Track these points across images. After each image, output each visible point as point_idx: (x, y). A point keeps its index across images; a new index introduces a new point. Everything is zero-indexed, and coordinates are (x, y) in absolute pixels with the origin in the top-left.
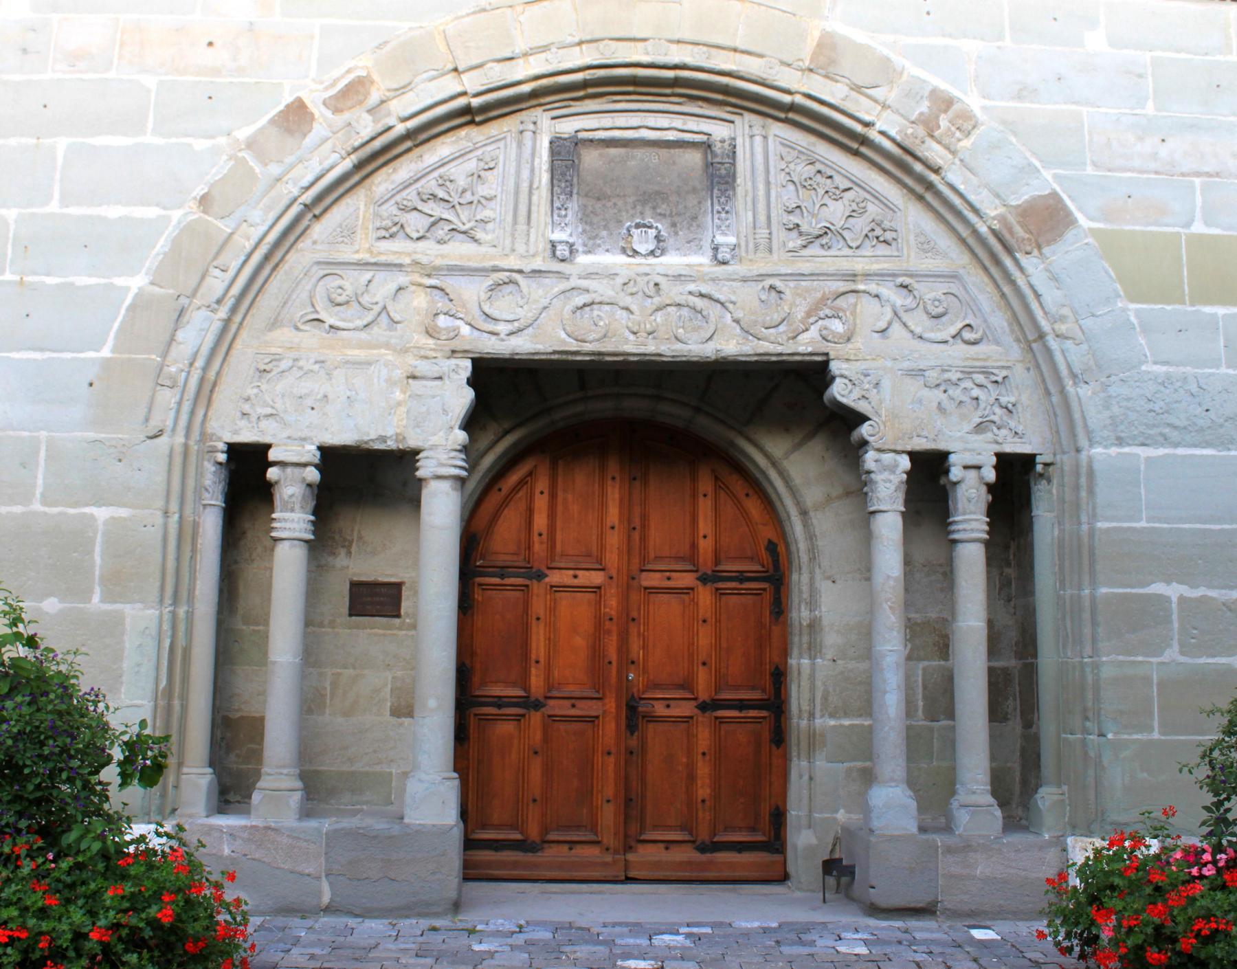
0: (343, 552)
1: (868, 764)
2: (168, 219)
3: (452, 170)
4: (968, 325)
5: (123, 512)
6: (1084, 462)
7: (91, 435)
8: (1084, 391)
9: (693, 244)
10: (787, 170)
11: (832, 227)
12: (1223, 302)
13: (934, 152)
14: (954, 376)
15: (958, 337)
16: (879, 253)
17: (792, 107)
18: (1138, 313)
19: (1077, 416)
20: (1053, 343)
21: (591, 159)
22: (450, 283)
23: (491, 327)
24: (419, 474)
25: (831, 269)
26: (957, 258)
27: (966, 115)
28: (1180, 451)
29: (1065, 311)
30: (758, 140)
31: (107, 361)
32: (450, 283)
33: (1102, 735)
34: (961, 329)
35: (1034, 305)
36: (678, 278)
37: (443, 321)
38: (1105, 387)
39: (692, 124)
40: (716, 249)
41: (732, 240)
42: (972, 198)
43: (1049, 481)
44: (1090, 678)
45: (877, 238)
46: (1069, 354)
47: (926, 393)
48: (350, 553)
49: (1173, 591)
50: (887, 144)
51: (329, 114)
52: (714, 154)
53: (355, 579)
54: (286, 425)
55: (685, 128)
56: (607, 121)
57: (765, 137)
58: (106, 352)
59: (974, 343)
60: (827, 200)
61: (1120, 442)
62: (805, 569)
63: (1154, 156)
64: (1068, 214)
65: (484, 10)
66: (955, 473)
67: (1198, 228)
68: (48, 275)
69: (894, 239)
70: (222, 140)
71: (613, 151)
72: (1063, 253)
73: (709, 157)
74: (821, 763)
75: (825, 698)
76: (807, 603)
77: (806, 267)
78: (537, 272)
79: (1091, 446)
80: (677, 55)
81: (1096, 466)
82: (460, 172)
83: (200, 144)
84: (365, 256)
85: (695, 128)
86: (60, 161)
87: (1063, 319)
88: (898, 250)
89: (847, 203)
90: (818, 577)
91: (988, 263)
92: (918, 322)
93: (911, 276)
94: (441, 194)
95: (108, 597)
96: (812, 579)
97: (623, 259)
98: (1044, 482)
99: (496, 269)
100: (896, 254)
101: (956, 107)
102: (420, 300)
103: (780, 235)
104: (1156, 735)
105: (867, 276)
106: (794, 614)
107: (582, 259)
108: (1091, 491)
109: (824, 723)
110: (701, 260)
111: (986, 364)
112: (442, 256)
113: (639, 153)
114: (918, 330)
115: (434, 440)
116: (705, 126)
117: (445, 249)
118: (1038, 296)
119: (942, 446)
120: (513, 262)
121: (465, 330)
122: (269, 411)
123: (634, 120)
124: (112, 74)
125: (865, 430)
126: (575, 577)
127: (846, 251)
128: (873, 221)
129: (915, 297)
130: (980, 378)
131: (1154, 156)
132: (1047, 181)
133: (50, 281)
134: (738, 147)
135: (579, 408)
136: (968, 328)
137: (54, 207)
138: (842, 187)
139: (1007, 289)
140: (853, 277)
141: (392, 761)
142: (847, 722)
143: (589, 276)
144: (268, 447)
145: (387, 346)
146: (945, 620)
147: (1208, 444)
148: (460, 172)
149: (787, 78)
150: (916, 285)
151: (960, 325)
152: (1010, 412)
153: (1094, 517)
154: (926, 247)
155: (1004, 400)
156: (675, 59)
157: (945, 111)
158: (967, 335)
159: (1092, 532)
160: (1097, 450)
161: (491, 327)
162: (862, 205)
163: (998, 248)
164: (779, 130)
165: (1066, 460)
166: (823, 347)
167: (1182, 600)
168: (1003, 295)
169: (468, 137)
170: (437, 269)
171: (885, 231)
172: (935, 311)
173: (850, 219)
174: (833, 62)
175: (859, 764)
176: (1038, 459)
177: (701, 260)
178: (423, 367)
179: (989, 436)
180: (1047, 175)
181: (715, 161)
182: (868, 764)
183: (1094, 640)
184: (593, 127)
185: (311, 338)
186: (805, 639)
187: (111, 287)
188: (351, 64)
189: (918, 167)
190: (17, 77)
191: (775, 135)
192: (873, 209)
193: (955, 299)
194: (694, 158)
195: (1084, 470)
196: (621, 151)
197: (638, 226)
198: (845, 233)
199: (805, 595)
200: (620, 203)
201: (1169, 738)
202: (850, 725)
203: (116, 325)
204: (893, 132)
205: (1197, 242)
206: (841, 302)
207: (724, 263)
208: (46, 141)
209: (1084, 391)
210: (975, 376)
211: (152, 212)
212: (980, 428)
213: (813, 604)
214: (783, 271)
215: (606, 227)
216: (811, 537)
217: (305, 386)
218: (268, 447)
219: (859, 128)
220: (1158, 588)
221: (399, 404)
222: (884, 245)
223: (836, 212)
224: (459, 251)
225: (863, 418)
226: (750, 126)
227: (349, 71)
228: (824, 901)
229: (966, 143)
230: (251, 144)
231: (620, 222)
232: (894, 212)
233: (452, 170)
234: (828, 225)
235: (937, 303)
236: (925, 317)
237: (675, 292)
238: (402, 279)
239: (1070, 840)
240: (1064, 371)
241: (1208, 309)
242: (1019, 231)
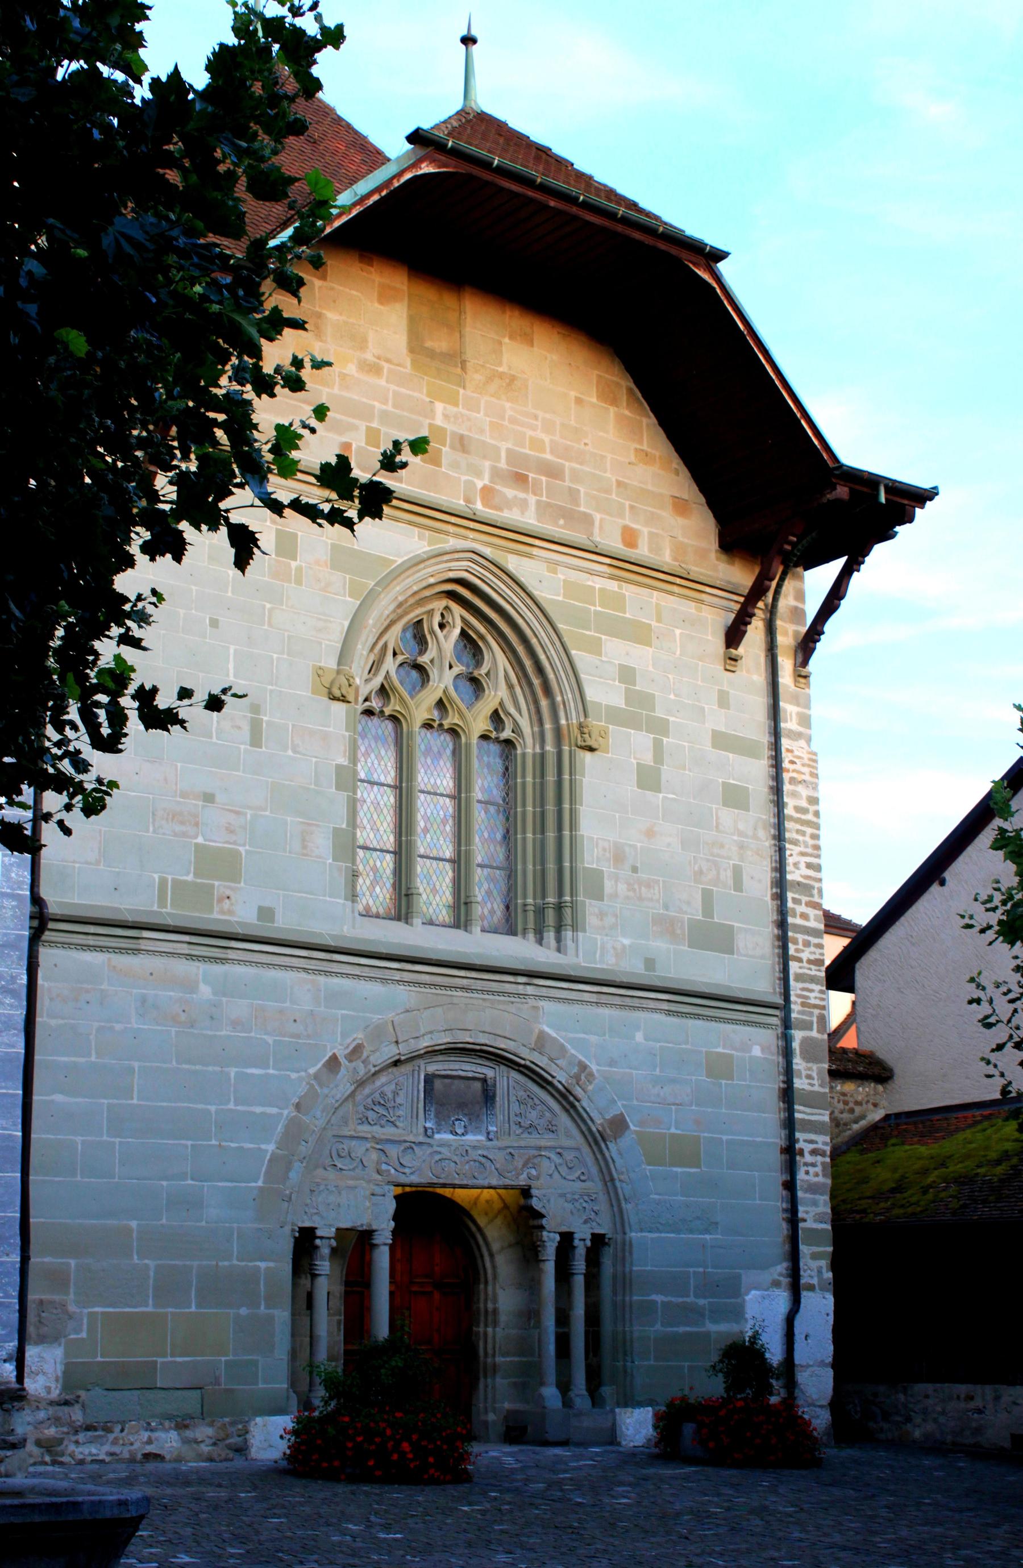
2: (282, 1114)
3: (385, 1089)
5: (271, 1264)
6: (627, 1239)
7: (256, 1225)
8: (629, 1206)
9: (477, 1130)
12: (680, 1166)
13: (578, 1091)
14: (576, 1197)
17: (525, 1066)
18: (650, 1170)
19: (626, 1217)
20: (618, 1184)
21: (438, 1084)
23: (402, 1170)
24: (374, 1242)
25: (533, 1145)
26: (580, 1140)
27: (591, 1075)
28: (663, 1235)
29: (624, 1170)
31: (260, 1188)
32: (388, 1148)
33: (633, 1362)
35: (612, 1166)
36: (474, 1147)
37: (384, 1167)
38: (637, 1205)
39: (480, 1069)
40: (488, 1133)
41: (495, 1129)
42: (592, 1115)
44: (628, 1337)
46: (624, 1189)
47: (566, 1204)
49: (659, 1298)
50: (560, 1087)
51: (347, 1062)
52: (487, 1085)
54: (322, 1217)
56: (446, 1066)
58: (260, 1183)
59: (584, 1181)
61: (642, 1231)
63: (658, 1095)
65: (408, 1011)
66: (576, 1242)
67: (673, 1130)
68: (232, 1142)
70: (303, 1074)
72: (626, 1141)
74: (498, 1380)
77: (522, 1143)
78: (421, 1143)
79: (631, 1231)
80: (483, 1039)
81: (633, 1242)
82: (388, 1090)
83: (294, 1076)
84: (352, 1133)
86: (233, 1081)
87: (622, 1173)
90: (497, 1287)
91: (592, 1144)
92: (563, 1170)
95: (267, 1307)
96: (494, 1289)
97: (451, 1137)
99: (405, 1141)
101: (588, 1070)
102: (374, 1156)
103: (514, 1127)
104: (652, 1362)
105: (546, 1148)
107: (437, 1136)
108: (631, 1253)
109: (499, 1359)
110: (482, 1138)
113: (456, 1082)
114: (564, 1174)
115: (384, 1226)
117: (384, 1130)
118: (614, 1161)
119: (572, 1230)
120: (411, 1138)
121: (393, 1171)
122: (315, 1211)
123: (457, 1066)
124: (252, 1034)
125: (544, 1222)
127: (538, 1136)
130: (586, 1198)
131: (658, 1095)
132: (619, 1107)
133: (233, 1145)
137: (231, 1106)
139: (599, 1157)
140: (540, 1148)
142: (508, 1359)
145: (363, 1179)
147: (672, 1232)
148: (388, 1090)
149: (525, 1053)
153: (632, 1264)
154: (568, 1135)
155: (595, 1208)
156: (483, 1041)
157: (583, 1072)
159: (631, 1271)
160: (633, 1234)
161: (402, 1170)
163: (599, 1138)
164: (514, 1074)
165: (619, 1237)
166: (530, 1182)
167: (662, 1302)
168: (597, 1159)
169: (392, 1073)
170: (381, 1140)
172: (570, 1165)
174: (543, 1046)
177: (482, 1138)
178: (378, 1190)
179: (589, 1225)
180: (619, 1104)
182: (566, 1330)
183: (631, 1320)
185: (331, 1174)
187: (260, 1149)
188: (355, 1036)
189: (571, 1098)
190: (209, 1033)
192: (548, 1114)
194: (478, 1085)
195: (627, 1243)
197: (457, 1120)
203: (264, 1169)
204: (563, 1082)
205: (673, 1136)
206: (536, 1161)
207: (491, 1140)
208: (226, 1069)
209: (629, 1206)
211: (274, 1110)
212: (585, 1222)
213: (495, 1300)
215: (444, 1120)
216: (494, 1267)
217: (332, 1199)
219: (550, 1078)
220: (654, 1297)
221: (368, 1208)
223: (533, 1115)
224: (389, 1131)
225: (543, 1216)
227: (354, 1040)
229: (590, 1088)
230: (316, 1076)
231: (449, 1117)
233: (385, 1089)
237: (474, 1154)
238: (368, 1145)
239: (617, 1410)
240: (621, 1197)
241: (675, 1169)
242: (608, 1131)
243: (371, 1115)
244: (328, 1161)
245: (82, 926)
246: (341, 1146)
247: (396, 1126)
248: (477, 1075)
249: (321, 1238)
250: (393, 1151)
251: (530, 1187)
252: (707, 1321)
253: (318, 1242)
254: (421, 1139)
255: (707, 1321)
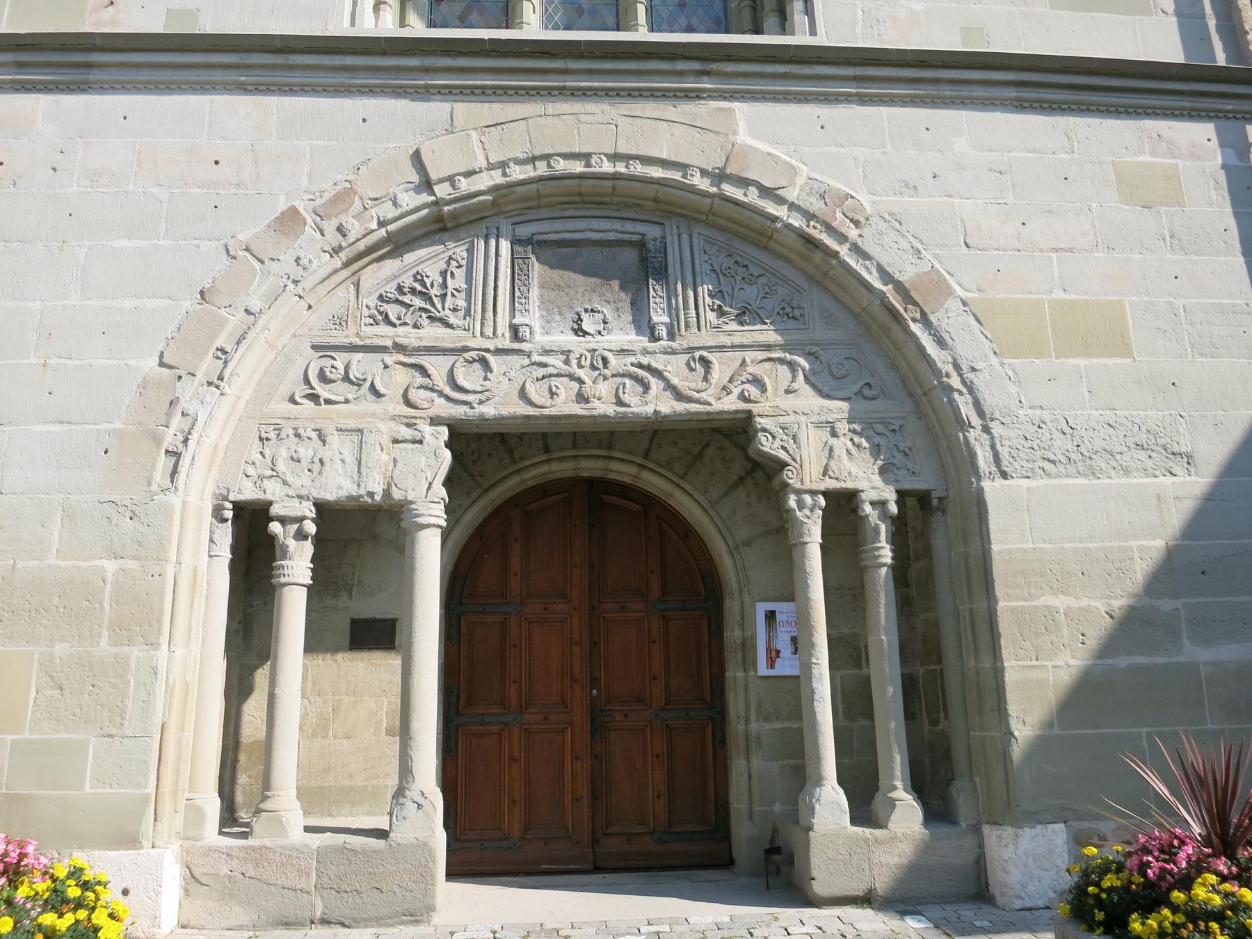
0: (344, 594)
1: (799, 761)
4: (868, 384)
10: (710, 261)
11: (748, 307)
15: (859, 394)
16: (789, 327)
22: (425, 361)
30: (685, 237)
32: (425, 361)
34: (862, 387)
36: (621, 352)
39: (629, 227)
43: (944, 512)
45: (787, 314)
48: (352, 595)
49: (1060, 602)
52: (648, 251)
53: (355, 617)
55: (623, 229)
57: (691, 236)
60: (743, 285)
62: (736, 595)
64: (949, 287)
67: (1058, 295)
69: (801, 315)
71: (564, 251)
73: (644, 253)
74: (756, 761)
75: (759, 705)
76: (740, 625)
77: (726, 340)
82: (432, 272)
85: (632, 230)
88: (805, 324)
89: (760, 287)
93: (817, 345)
94: (419, 288)
95: (114, 643)
98: (939, 514)
100: (802, 327)
102: (402, 377)
106: (727, 634)
111: (884, 415)
112: (420, 339)
116: (640, 228)
123: (581, 224)
126: (515, 575)
128: (783, 301)
129: (821, 362)
130: (880, 428)
134: (668, 244)
135: (544, 469)
136: (867, 386)
138: (756, 273)
141: (387, 775)
143: (547, 352)
144: (270, 503)
146: (857, 635)
150: (821, 352)
151: (860, 384)
152: (907, 455)
155: (902, 446)
158: (867, 392)
162: (773, 288)
166: (742, 406)
171: (793, 308)
173: (765, 300)
175: (791, 762)
176: (934, 494)
181: (649, 255)
182: (799, 761)
184: (547, 230)
186: (739, 656)
191: (699, 234)
192: (782, 291)
193: (855, 363)
196: (571, 250)
198: (759, 311)
199: (738, 618)
200: (572, 292)
201: (1067, 732)
202: (781, 728)
210: (876, 426)
214: (709, 344)
218: (270, 503)
220: (1048, 600)
222: (791, 321)
224: (432, 334)
226: (678, 227)
228: (768, 888)
232: (800, 292)
234: (745, 305)
235: (840, 367)
236: (830, 379)
243: (393, 311)
244: (303, 390)
245: (488, 296)
246: (330, 362)
247: (448, 325)
248: (626, 237)
249: (283, 520)
250: (438, 367)
251: (749, 416)
252: (1186, 641)
253: (275, 527)
254: (506, 343)
255: (1186, 641)
